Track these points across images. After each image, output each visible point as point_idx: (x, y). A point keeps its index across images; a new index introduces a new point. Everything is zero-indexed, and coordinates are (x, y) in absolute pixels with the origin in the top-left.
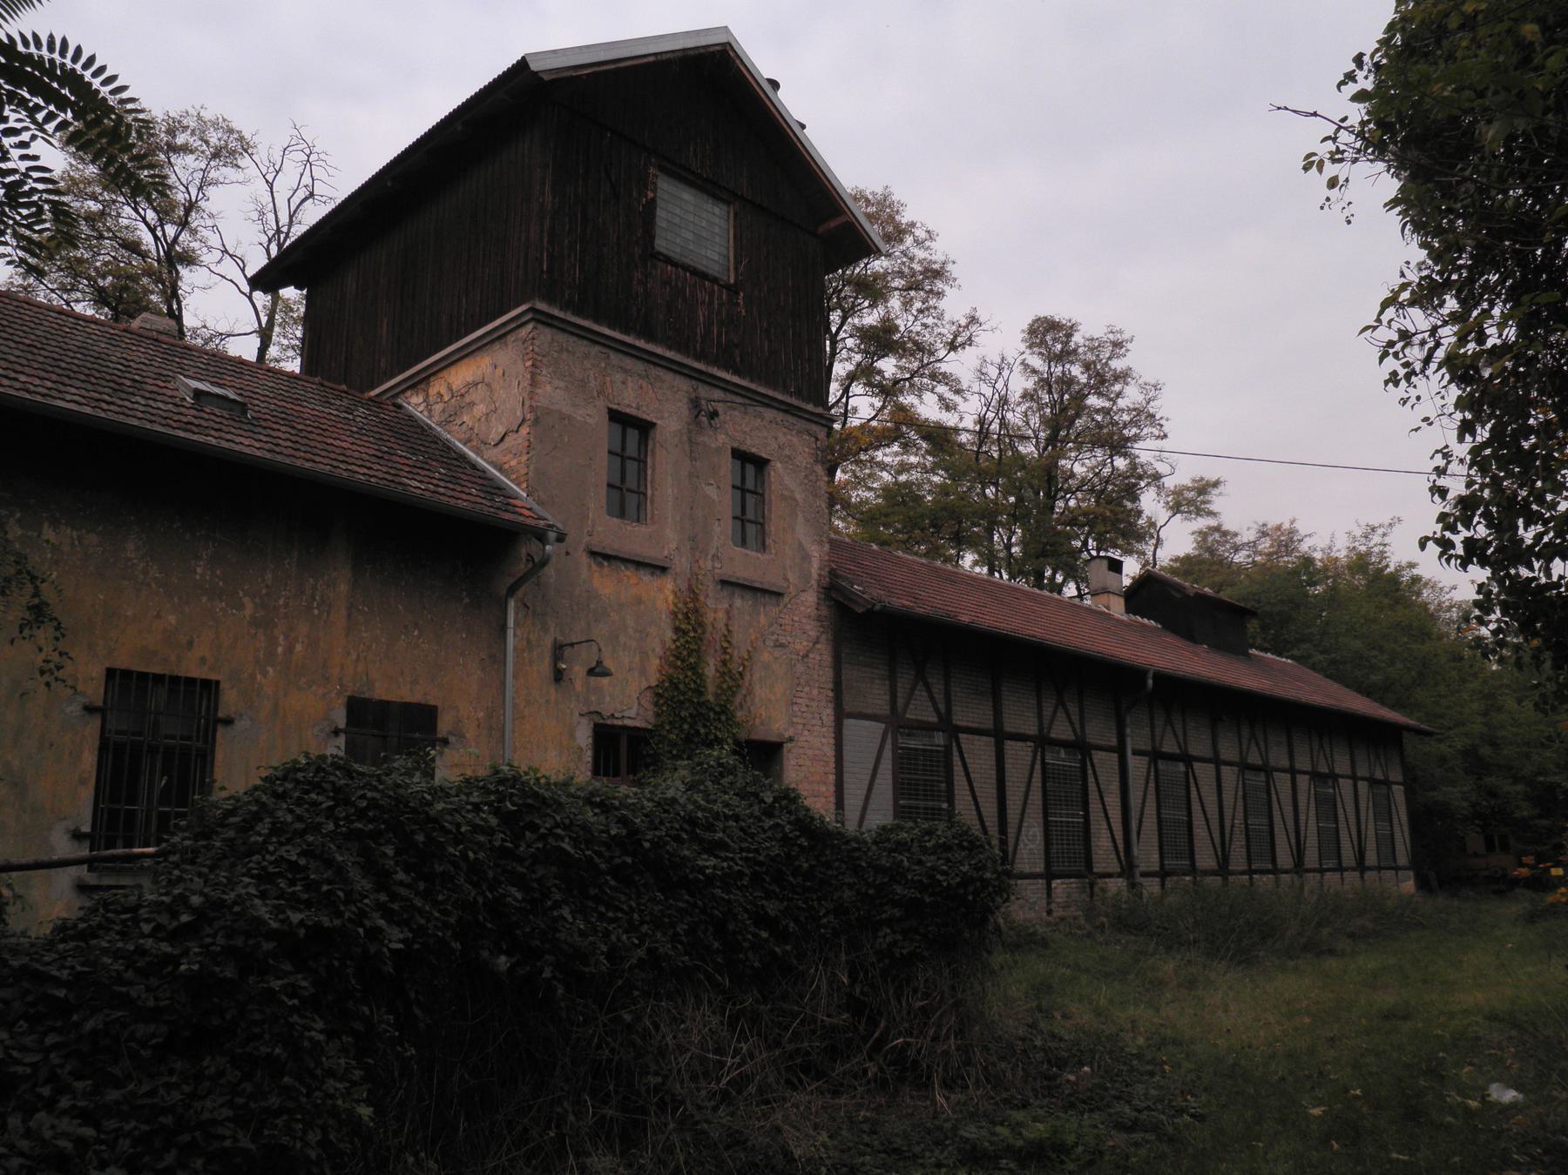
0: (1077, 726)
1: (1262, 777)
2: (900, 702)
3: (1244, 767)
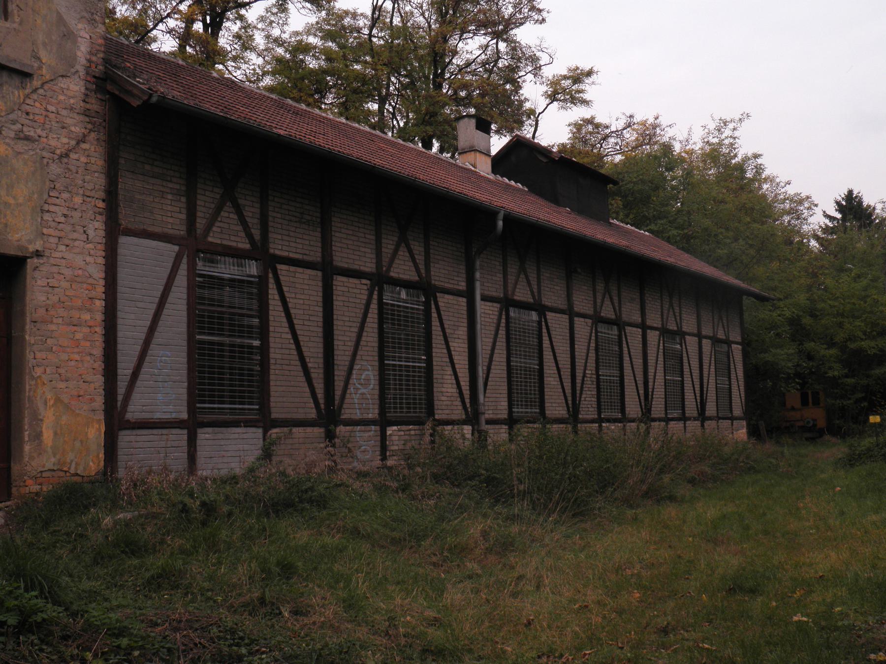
0: (422, 267)
1: (615, 331)
2: (201, 223)
3: (598, 320)
